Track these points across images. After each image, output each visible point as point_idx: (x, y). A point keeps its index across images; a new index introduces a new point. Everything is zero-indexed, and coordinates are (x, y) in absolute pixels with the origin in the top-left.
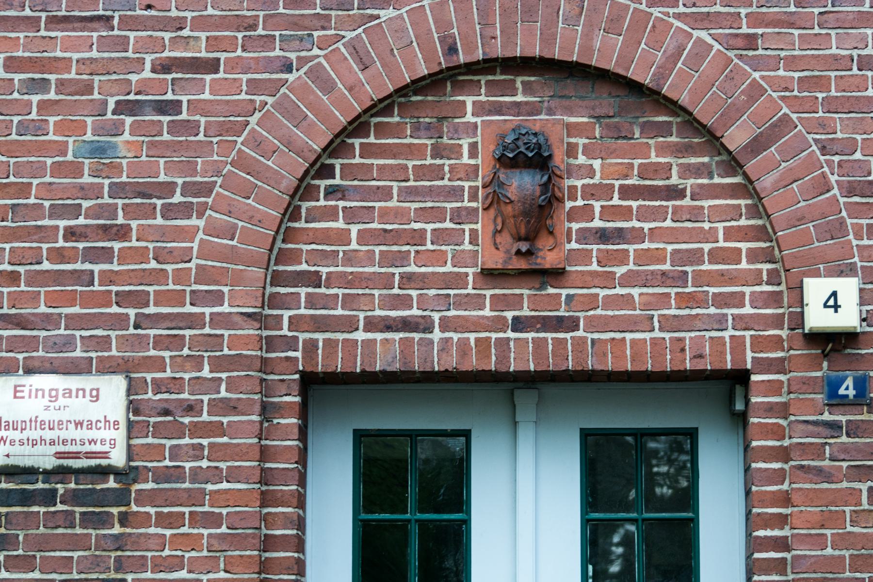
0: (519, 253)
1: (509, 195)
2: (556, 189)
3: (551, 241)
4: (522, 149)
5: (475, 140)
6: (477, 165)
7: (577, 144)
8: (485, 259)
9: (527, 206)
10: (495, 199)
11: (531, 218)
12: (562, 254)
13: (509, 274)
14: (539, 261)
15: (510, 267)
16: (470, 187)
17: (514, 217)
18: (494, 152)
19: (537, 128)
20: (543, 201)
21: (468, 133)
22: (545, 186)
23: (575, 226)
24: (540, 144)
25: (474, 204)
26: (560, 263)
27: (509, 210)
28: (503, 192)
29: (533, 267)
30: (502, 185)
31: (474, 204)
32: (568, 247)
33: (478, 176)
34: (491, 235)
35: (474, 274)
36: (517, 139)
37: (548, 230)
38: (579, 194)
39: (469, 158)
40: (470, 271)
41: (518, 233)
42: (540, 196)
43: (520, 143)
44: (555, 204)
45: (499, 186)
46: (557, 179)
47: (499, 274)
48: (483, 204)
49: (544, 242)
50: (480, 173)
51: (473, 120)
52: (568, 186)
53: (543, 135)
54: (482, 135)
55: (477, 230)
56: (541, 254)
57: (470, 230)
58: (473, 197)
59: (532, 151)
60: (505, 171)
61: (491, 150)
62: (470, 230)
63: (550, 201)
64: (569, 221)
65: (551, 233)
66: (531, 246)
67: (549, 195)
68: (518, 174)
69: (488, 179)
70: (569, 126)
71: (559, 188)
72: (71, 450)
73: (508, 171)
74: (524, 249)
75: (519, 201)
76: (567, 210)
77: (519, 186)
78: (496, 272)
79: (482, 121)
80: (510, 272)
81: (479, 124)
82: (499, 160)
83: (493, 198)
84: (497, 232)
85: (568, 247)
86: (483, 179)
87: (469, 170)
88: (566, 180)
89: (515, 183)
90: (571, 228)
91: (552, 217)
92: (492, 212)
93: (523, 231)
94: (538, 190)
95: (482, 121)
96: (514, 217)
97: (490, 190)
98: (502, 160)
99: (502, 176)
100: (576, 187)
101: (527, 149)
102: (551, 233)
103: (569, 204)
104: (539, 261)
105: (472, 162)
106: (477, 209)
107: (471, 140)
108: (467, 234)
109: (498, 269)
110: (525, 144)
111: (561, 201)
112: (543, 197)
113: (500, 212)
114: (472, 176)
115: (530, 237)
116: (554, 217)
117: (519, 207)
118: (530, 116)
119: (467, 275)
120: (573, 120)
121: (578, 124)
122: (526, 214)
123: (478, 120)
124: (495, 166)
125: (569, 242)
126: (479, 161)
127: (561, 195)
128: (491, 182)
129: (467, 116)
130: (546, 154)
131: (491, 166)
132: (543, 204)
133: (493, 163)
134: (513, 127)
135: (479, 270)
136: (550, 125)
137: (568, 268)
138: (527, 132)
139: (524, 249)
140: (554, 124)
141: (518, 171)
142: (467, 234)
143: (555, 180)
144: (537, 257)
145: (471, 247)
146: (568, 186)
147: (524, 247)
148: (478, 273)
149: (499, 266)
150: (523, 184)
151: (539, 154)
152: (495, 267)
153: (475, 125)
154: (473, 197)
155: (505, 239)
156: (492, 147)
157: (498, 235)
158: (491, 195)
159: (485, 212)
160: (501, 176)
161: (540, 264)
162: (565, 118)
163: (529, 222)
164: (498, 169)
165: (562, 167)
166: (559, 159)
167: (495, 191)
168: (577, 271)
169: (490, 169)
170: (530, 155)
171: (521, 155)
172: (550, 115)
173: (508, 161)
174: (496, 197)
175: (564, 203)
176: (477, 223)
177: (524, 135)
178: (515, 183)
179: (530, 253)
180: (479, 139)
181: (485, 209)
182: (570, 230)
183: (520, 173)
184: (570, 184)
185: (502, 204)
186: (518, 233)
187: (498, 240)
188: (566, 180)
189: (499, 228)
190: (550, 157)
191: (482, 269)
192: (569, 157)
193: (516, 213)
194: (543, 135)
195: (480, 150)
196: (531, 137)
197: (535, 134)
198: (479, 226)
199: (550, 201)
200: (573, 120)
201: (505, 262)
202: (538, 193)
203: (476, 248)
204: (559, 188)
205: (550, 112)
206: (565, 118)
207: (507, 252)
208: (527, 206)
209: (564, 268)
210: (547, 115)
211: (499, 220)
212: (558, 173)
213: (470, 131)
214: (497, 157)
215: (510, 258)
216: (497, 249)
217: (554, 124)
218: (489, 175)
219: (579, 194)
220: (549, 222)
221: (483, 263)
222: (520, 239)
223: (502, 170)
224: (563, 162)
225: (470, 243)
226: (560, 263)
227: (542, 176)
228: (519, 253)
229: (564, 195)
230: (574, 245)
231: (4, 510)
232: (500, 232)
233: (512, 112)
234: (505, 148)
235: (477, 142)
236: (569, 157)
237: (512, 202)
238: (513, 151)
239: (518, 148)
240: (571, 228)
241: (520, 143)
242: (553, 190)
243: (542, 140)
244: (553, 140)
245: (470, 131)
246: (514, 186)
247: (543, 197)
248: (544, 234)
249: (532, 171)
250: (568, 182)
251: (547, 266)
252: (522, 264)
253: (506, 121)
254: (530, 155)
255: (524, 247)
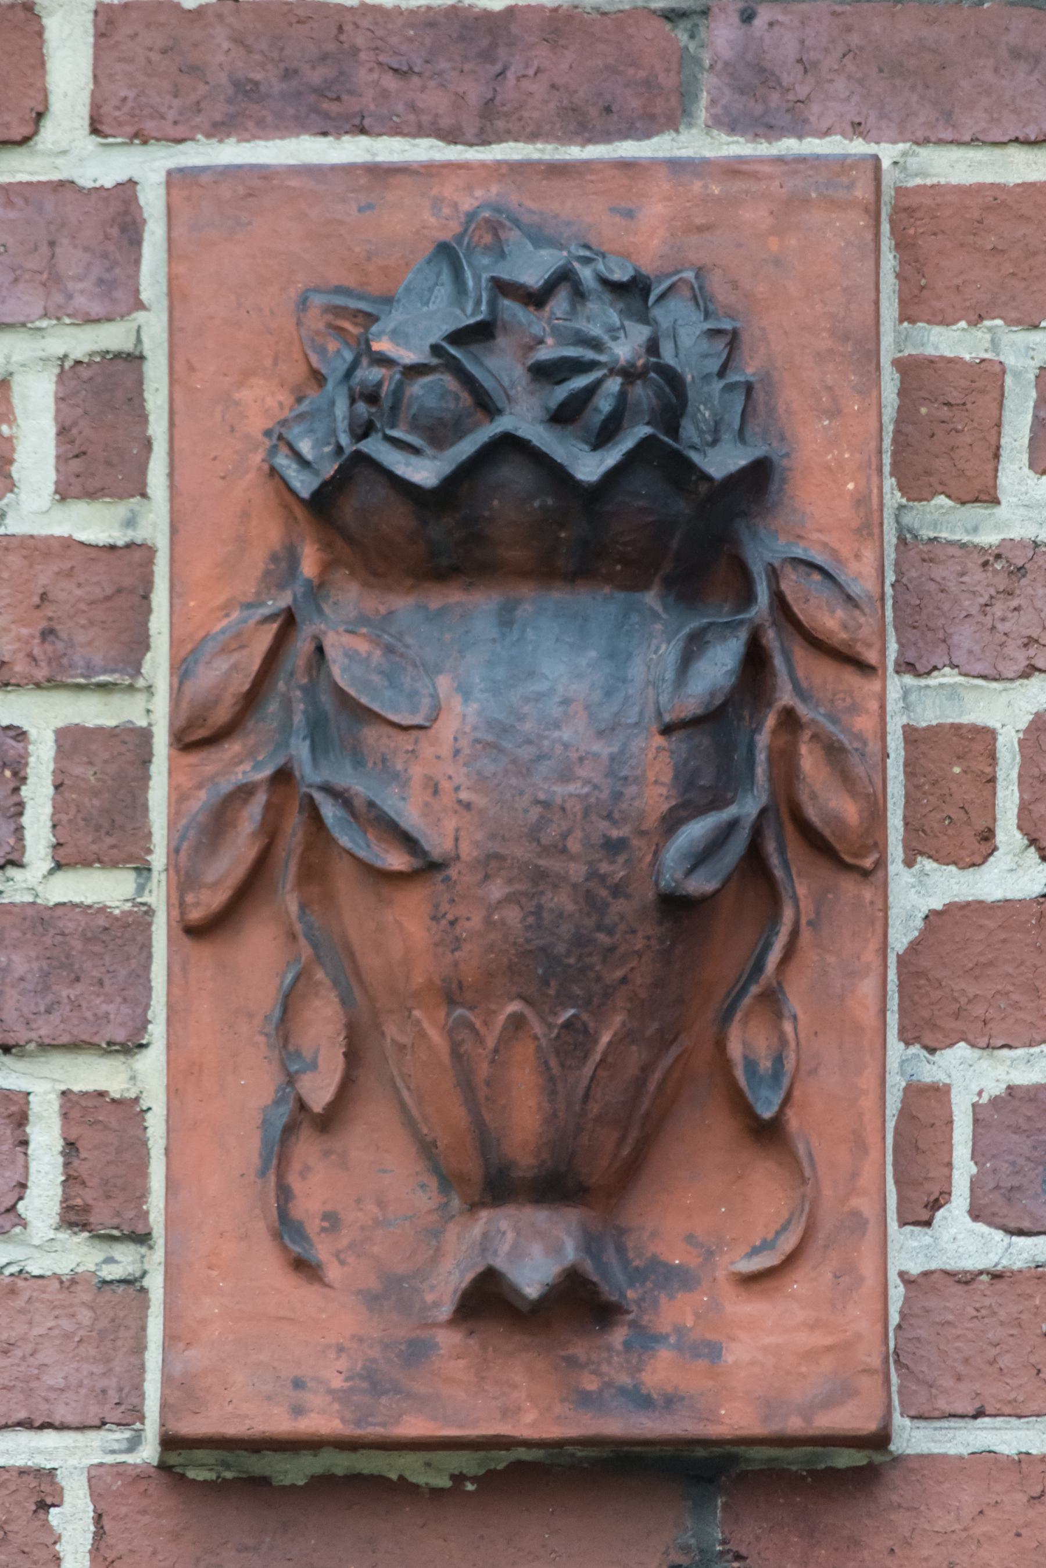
0: (487, 1301)
1: (410, 815)
2: (809, 760)
3: (763, 1205)
4: (524, 418)
5: (112, 337)
6: (138, 554)
7: (989, 377)
8: (196, 1357)
9: (562, 900)
10: (289, 847)
11: (598, 1002)
12: (858, 1319)
13: (404, 1488)
14: (661, 1371)
15: (415, 1426)
16: (72, 741)
17: (452, 993)
18: (279, 439)
19: (645, 240)
20: (703, 856)
21: (52, 279)
22: (717, 734)
23: (972, 1075)
24: (672, 378)
25: (106, 889)
26: (842, 1393)
27: (404, 933)
28: (359, 787)
29: (615, 1425)
30: (339, 721)
31: (106, 889)
32: (910, 1251)
33: (140, 643)
34: (246, 1148)
35: (98, 1480)
36: (479, 334)
37: (740, 1106)
38: (1008, 799)
39: (63, 493)
40: (73, 1456)
41: (484, 1139)
42: (672, 823)
43: (502, 367)
44: (802, 885)
45: (318, 731)
46: (821, 674)
47: (324, 1484)
48: (184, 881)
49: (703, 1214)
50: (159, 623)
51: (102, 166)
52: (912, 736)
53: (701, 299)
54: (176, 294)
55: (130, 1110)
56: (675, 1312)
57: (72, 1103)
58: (99, 829)
59: (603, 436)
60: (375, 603)
61: (256, 424)
62: (72, 1103)
63: (754, 858)
64: (925, 1031)
65: (767, 1134)
66: (591, 1244)
67: (747, 807)
68: (484, 626)
69: (226, 674)
70: (919, 224)
71: (834, 752)
72: (889, 1053)
73: (402, 604)
74: (532, 1275)
75: (490, 863)
76: (901, 936)
77: (495, 737)
78: (293, 1471)
79: (179, 180)
80: (411, 1467)
81: (152, 201)
82: (322, 505)
83: (270, 833)
84: (302, 1124)
85: (910, 1251)
86: (182, 669)
87: (66, 592)
88: (895, 685)
89: (460, 716)
90: (940, 1093)
91: (772, 1000)
92: (260, 952)
93: (524, 1120)
94: (655, 773)
95: (179, 180)
96: (452, 993)
97: (242, 764)
98: (348, 510)
99: (348, 642)
100: (986, 735)
101: (563, 416)
102: (767, 1134)
103: (917, 891)
104: (661, 1371)
105: (94, 524)
106: (138, 921)
107: (82, 342)
108: (46, 1137)
109: (313, 1445)
110: (546, 373)
111: (846, 857)
112: (697, 830)
113: (329, 956)
114: (89, 644)
115: (581, 1174)
116: (796, 1000)
117: (488, 911)
118: (585, 133)
119: (41, 1490)
120: (954, 167)
121: (995, 201)
122: (552, 969)
123: (148, 168)
124: (287, 560)
125: (923, 1210)
126: (154, 524)
127: (850, 811)
128: (252, 699)
129: (49, 134)
130: (722, 461)
131: (256, 560)
132: (700, 885)
133: (269, 532)
134: (443, 227)
135: (148, 1453)
136: (755, 215)
137: (912, 1438)
138: (564, 277)
139: (532, 1275)
140: (796, 203)
141: (481, 604)
142: (46, 1137)
143: (799, 680)
144: (646, 1340)
145: (77, 1255)
146: (912, 736)
147: (535, 1253)
148: (138, 1477)
149: (322, 1421)
150: (528, 713)
151: (665, 460)
152: (279, 1423)
153: (121, 207)
154: (99, 829)
155: (374, 1186)
156: (263, 402)
157: (307, 1149)
158: (252, 813)
159: (203, 953)
160: (336, 644)
161: (671, 1402)
162: (888, 153)
163: (575, 1039)
164: (316, 592)
165: (860, 574)
166: (836, 506)
167: (283, 777)
168: (987, 1460)
169: (247, 585)
170: (589, 467)
171: (513, 475)
172: (765, 127)
173: (399, 517)
174: (294, 824)
175: (873, 874)
176: (132, 1046)
177: (536, 299)
178: (460, 716)
179: (580, 1305)
180: (152, 328)
181: (199, 931)
182: (927, 1103)
183: (506, 619)
184: (930, 714)
185: (346, 884)
186: (484, 1139)
187: (312, 1197)
188: (895, 685)
189: (319, 1090)
190: (758, 479)
191: (169, 1442)
192: (916, 483)
193: (470, 959)
194: (701, 299)
195: (158, 428)
196: (600, 316)
197: (633, 292)
198: (147, 1077)
199: (754, 858)
200: (954, 167)
201: (372, 1382)
202: (655, 797)
203: (125, 1261)
204: (834, 752)
205: (761, 99)
206: (888, 153)
207: (392, 1293)
208: (562, 900)
209: (880, 1440)
210: (731, 123)
211: (322, 1026)
212: (829, 619)
213: (71, 260)
214: (304, 484)
215: (416, 1353)
216: (304, 1267)
217: (796, 203)
218: (237, 641)
219: (1008, 799)
220: (747, 1041)
221: (180, 1390)
222: (498, 1187)
223: (350, 597)
224: (868, 528)
225: (74, 1217)
226: (842, 1393)
227: (693, 648)
228: (487, 1301)
229: (876, 814)
230: (961, 1241)
231: (1007, 876)
232: (327, 1122)
233: (435, 101)
234: (375, 407)
235: (134, 359)
236: (916, 483)
237: (429, 867)
238: (439, 433)
239: (486, 405)
240: (940, 1093)
241: (502, 367)
242: (785, 765)
243: (688, 346)
244: (786, 343)
245: (71, 260)
246: (447, 729)
247: (697, 830)
248: (704, 1137)
249: (599, 604)
250: (912, 702)
251: (734, 1418)
252: (519, 1401)
253: (380, 173)
254: (589, 467)
255: (535, 1253)
